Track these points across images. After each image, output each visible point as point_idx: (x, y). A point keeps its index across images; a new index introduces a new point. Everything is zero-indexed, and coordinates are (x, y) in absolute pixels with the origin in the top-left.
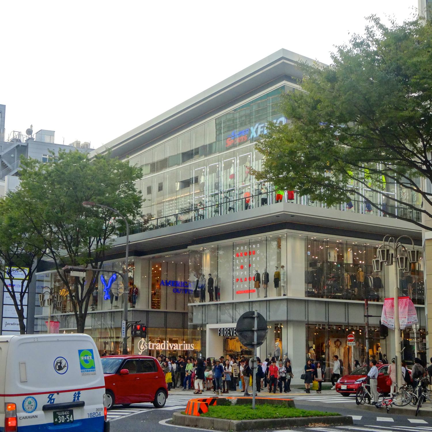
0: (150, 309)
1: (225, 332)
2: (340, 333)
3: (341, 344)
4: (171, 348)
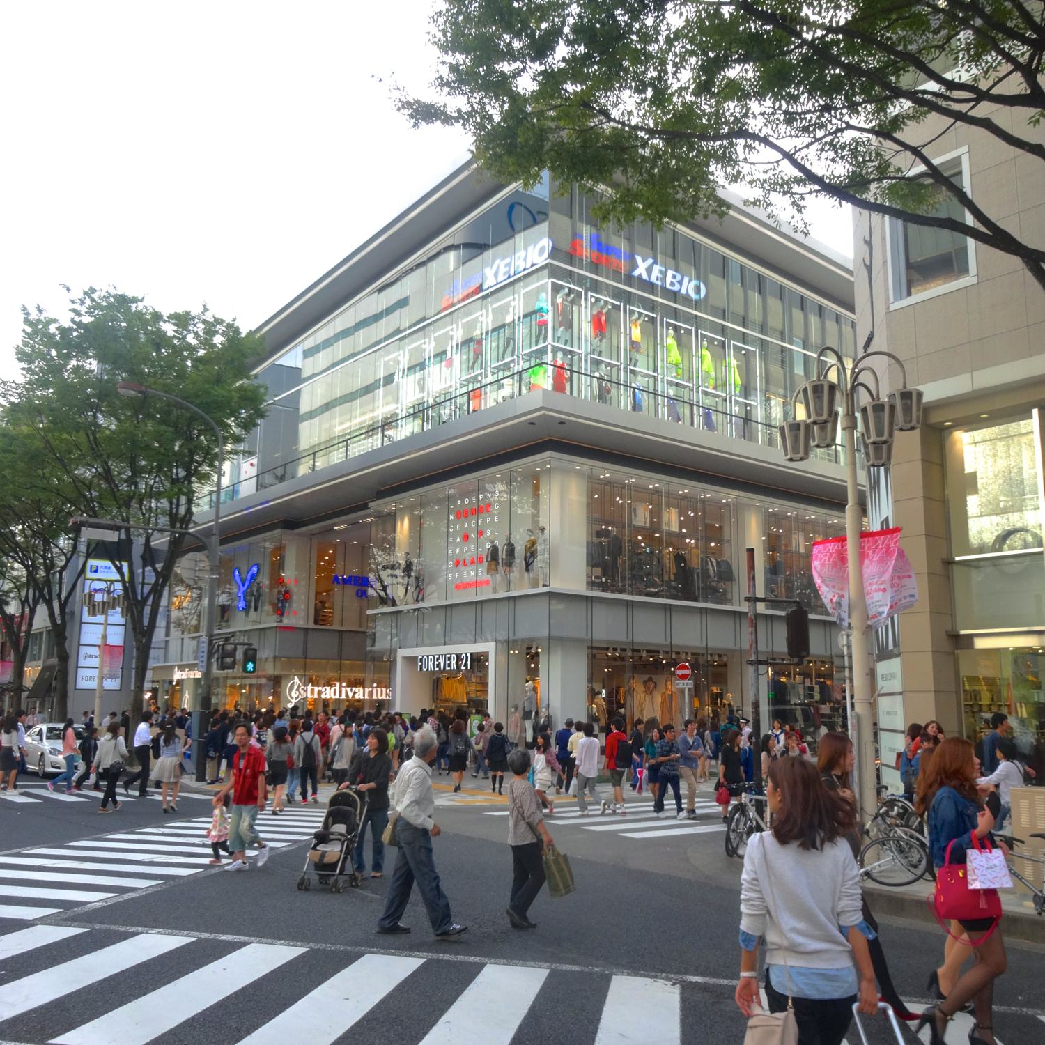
0: (311, 625)
1: (431, 663)
2: (651, 664)
3: (655, 687)
4: (350, 695)
